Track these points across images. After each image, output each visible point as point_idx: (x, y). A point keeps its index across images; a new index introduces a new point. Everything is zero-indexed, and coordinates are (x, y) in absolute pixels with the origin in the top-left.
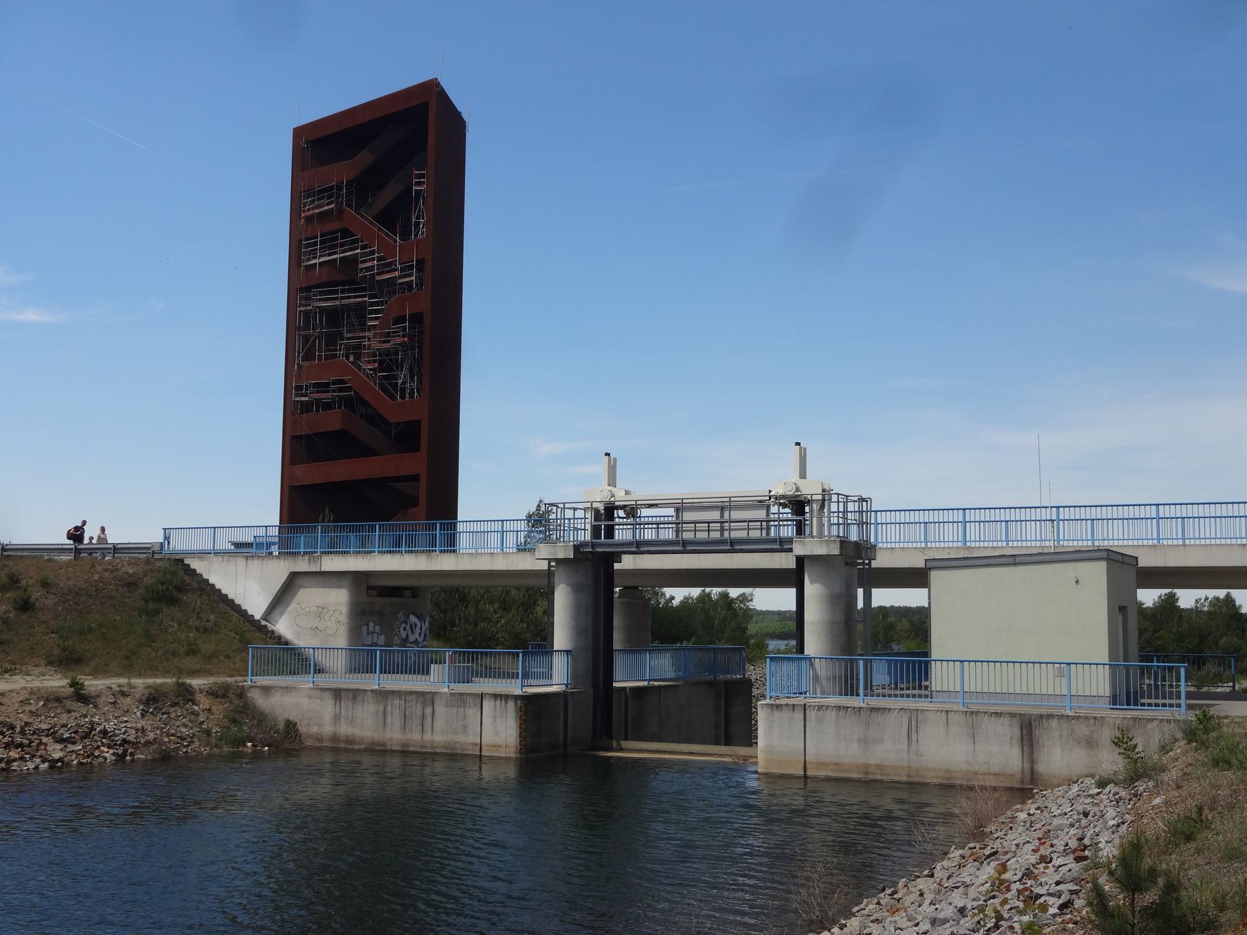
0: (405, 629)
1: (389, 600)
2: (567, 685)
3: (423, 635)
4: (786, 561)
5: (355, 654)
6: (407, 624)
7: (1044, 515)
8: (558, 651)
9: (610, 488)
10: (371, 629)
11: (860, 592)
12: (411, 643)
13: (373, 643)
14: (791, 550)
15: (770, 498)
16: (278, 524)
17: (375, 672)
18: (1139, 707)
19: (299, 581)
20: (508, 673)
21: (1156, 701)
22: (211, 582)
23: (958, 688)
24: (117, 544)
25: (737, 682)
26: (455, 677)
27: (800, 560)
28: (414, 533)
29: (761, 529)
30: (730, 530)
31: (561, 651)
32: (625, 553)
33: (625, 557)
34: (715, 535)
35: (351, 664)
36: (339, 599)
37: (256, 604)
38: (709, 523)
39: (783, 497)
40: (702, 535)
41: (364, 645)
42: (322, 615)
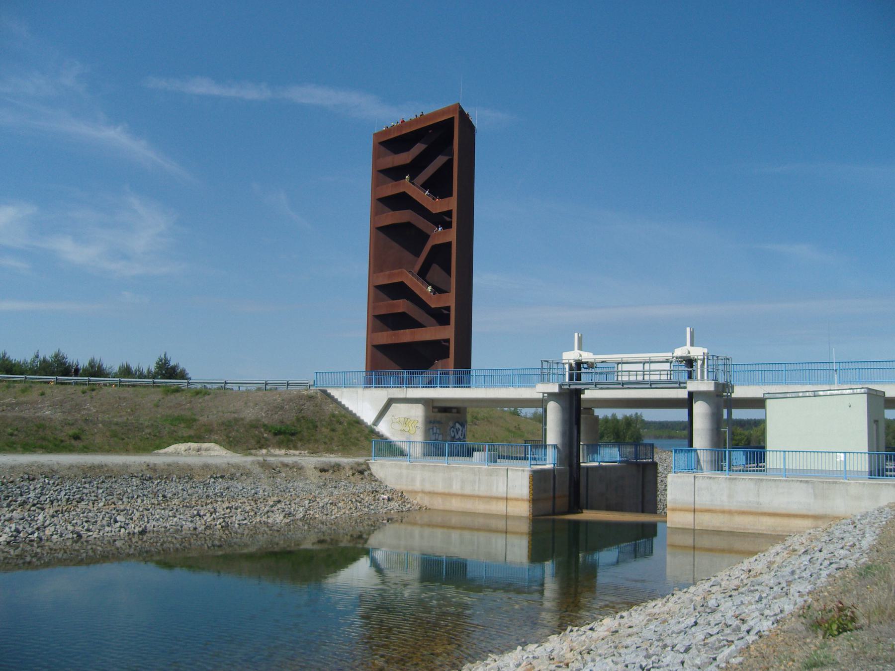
0: (453, 432)
1: (444, 415)
2: (554, 465)
3: (463, 435)
4: (682, 394)
5: (427, 445)
6: (454, 428)
7: (754, 367)
8: (550, 445)
9: (579, 351)
10: (435, 431)
11: (725, 411)
12: (457, 439)
13: (436, 439)
14: (685, 388)
15: (673, 358)
16: (365, 370)
17: (445, 456)
18: (885, 477)
19: (394, 406)
20: (515, 457)
21: (750, 466)
22: (343, 403)
23: (843, 469)
24: (267, 381)
25: (647, 463)
26: (491, 459)
27: (691, 394)
28: (458, 375)
29: (667, 374)
30: (622, 375)
31: (551, 445)
32: (587, 389)
33: (586, 391)
34: (640, 378)
35: (424, 450)
36: (417, 412)
37: (367, 415)
38: (637, 372)
39: (681, 357)
40: (633, 378)
41: (431, 441)
42: (407, 423)
